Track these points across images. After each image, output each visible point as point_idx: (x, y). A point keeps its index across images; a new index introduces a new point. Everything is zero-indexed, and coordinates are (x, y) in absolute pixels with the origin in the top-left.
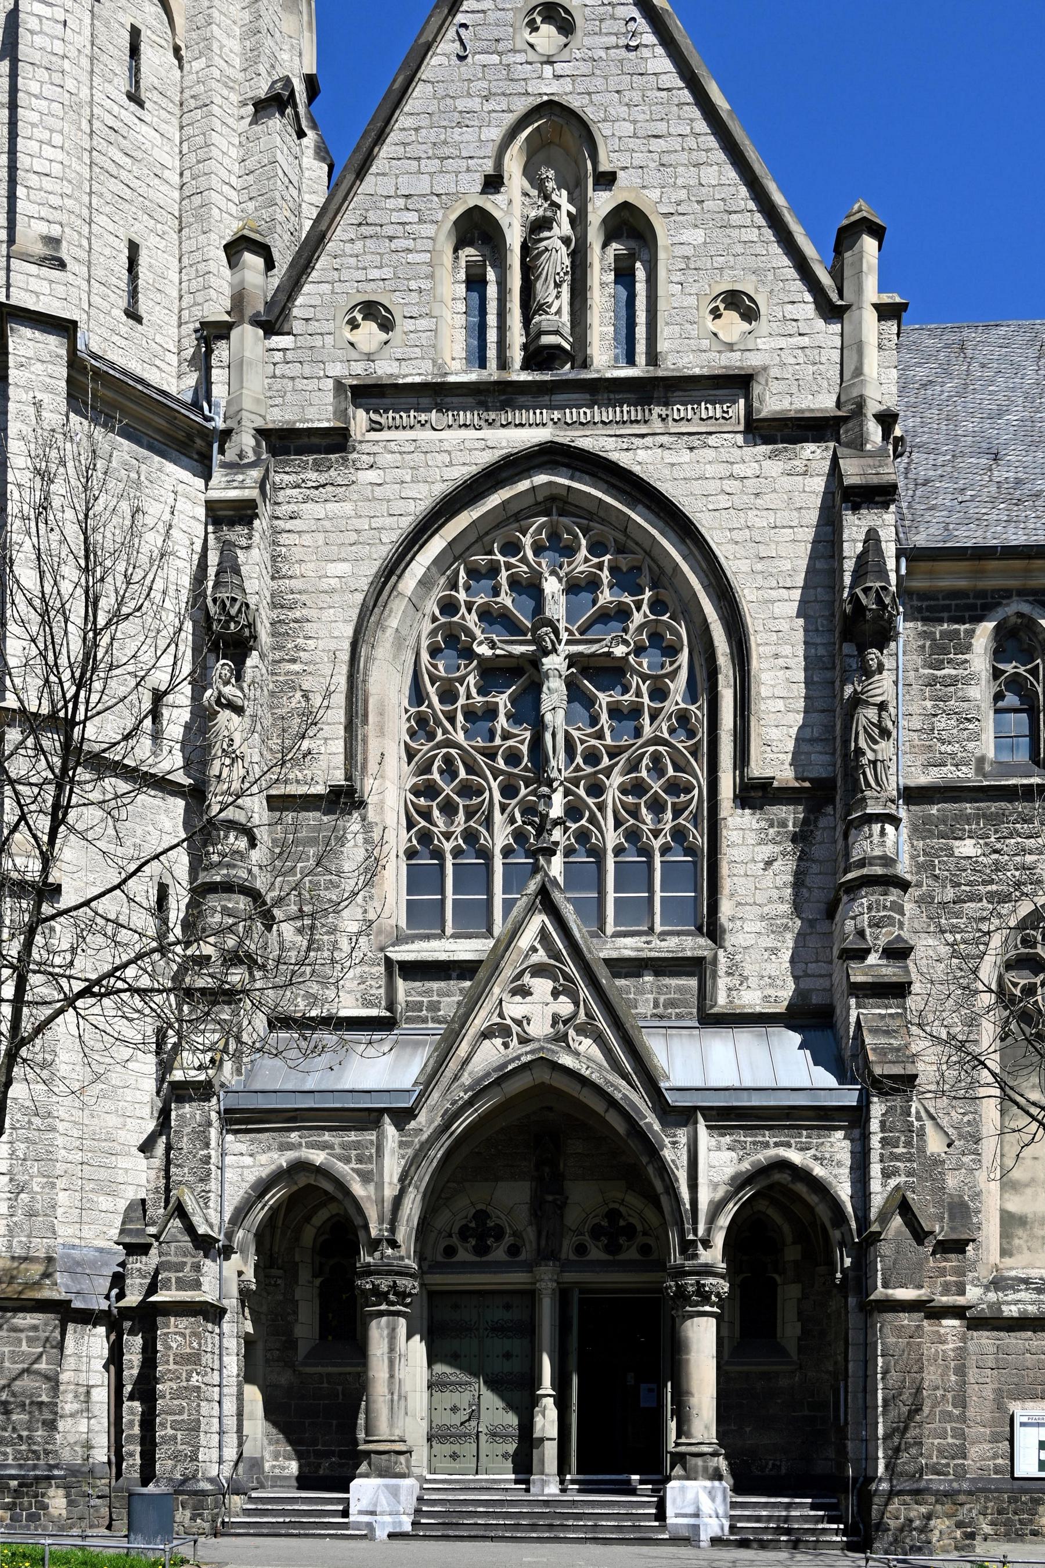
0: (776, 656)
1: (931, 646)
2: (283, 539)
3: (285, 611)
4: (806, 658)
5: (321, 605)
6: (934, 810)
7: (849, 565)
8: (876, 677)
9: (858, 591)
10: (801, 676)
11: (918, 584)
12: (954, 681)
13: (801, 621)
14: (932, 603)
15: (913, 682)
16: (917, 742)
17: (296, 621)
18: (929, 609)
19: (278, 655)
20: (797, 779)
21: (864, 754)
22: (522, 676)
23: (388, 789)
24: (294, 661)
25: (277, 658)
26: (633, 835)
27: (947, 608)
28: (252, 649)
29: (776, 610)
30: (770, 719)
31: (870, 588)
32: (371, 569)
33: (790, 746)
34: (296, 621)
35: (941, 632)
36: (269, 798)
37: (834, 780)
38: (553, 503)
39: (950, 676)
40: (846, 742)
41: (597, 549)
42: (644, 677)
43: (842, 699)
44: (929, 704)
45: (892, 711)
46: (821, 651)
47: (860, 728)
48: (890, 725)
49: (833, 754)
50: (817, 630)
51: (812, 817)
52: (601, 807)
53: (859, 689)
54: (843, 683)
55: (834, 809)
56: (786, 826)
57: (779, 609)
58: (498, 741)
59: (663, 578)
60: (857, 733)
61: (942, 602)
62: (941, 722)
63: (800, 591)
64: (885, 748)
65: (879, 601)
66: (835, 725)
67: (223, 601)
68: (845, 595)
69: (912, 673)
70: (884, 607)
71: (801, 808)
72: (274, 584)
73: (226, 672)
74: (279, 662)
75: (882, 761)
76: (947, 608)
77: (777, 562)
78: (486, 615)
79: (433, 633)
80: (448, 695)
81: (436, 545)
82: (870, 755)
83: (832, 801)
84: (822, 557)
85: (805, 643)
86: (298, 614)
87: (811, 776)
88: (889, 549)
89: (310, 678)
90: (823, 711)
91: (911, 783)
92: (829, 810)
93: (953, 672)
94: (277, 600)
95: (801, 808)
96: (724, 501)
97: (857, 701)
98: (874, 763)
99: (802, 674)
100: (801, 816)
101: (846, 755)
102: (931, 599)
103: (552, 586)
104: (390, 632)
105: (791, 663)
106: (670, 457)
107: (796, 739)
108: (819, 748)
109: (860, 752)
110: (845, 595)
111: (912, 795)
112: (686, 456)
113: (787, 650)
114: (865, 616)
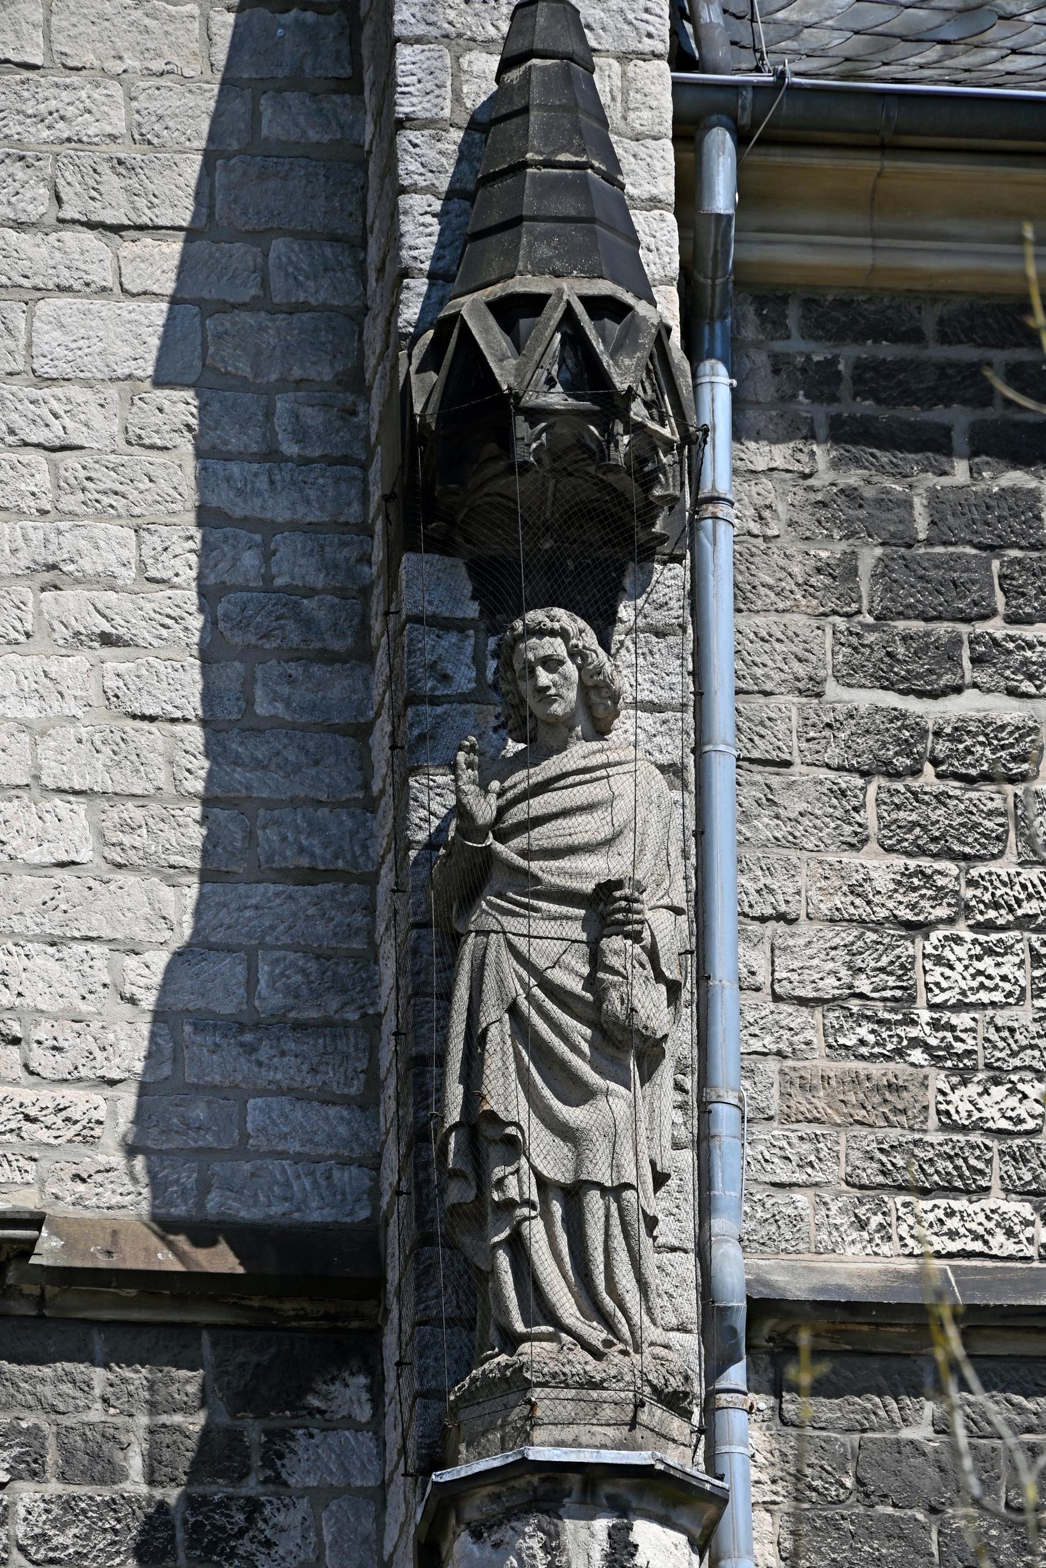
0: (51, 575)
1: (882, 571)
4: (209, 595)
7: (428, 161)
8: (578, 753)
9: (471, 307)
10: (185, 687)
11: (803, 253)
13: (181, 405)
14: (888, 351)
15: (794, 748)
16: (819, 1062)
18: (870, 378)
20: (165, 1226)
21: (514, 1147)
29: (48, 339)
31: (536, 303)
33: (129, 1047)
35: (935, 499)
37: (367, 1241)
39: (990, 730)
40: (422, 1069)
43: (400, 841)
44: (880, 867)
45: (669, 931)
46: (295, 564)
47: (492, 1012)
48: (651, 1006)
49: (367, 1103)
50: (271, 455)
51: (254, 1433)
53: (484, 809)
54: (411, 756)
55: (376, 1394)
56: (114, 1474)
57: (59, 331)
60: (476, 1040)
61: (937, 352)
62: (951, 968)
63: (174, 248)
64: (633, 1124)
65: (585, 373)
66: (372, 955)
68: (410, 312)
69: (789, 703)
70: (611, 405)
71: (188, 1382)
75: (616, 1191)
77: (49, 94)
82: (546, 1154)
83: (360, 1350)
84: (296, 82)
85: (205, 516)
87: (246, 1213)
88: (639, 97)
90: (309, 876)
91: (793, 1279)
92: (349, 1395)
93: (1009, 711)
95: (188, 1382)
97: (471, 872)
98: (573, 1194)
99: (190, 682)
100: (195, 1423)
101: (421, 1135)
102: (878, 332)
105: (127, 611)
107: (159, 1016)
108: (287, 1069)
109: (488, 1137)
110: (410, 312)
111: (789, 1340)
113: (108, 546)
114: (506, 440)
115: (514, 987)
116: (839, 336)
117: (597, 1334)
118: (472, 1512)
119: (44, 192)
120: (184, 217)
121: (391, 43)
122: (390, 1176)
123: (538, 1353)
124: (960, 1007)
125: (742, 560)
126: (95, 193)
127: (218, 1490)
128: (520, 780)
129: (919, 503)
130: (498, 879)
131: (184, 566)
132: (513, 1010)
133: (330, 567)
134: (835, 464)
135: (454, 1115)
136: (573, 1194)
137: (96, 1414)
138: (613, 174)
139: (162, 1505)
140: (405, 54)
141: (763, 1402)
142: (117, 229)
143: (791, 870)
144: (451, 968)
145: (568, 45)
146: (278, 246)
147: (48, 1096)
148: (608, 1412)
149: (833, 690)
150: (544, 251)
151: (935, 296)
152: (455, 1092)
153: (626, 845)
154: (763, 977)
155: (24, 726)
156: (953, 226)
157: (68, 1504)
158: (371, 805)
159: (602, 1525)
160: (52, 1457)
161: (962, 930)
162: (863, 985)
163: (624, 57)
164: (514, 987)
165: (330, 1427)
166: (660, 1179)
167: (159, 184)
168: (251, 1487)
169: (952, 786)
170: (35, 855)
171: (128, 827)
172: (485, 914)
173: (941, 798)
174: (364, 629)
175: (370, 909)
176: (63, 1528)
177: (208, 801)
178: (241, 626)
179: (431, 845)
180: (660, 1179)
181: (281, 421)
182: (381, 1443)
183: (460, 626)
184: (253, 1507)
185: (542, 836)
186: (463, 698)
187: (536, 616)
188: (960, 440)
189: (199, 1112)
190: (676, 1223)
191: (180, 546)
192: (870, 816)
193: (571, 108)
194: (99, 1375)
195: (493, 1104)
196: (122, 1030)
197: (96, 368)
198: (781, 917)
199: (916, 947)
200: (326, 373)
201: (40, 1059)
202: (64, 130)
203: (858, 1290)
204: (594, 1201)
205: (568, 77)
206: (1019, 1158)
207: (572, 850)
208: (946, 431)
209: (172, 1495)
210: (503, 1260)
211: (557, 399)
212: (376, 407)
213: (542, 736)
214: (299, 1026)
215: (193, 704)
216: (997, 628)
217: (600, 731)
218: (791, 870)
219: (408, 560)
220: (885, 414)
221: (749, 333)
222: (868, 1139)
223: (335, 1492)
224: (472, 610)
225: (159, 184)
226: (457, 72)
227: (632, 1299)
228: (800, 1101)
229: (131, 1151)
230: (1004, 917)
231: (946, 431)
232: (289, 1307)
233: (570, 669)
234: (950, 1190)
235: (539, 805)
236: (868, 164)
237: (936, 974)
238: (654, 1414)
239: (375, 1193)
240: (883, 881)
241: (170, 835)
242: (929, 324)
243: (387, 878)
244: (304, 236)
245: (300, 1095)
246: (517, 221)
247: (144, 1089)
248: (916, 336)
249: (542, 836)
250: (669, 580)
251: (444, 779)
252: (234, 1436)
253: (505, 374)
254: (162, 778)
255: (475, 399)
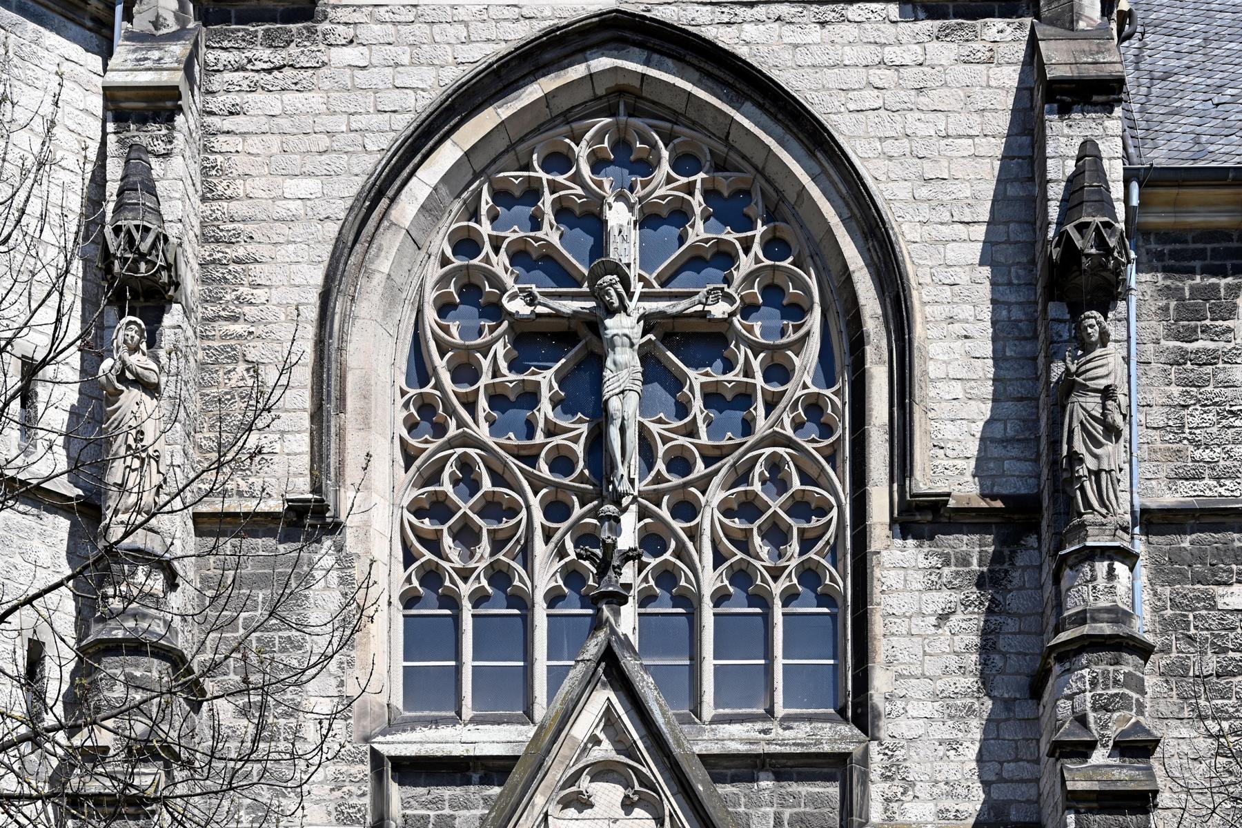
0: (951, 320)
1: (1177, 308)
2: (219, 143)
3: (222, 247)
4: (994, 323)
5: (276, 239)
6: (1186, 542)
7: (1056, 192)
8: (1098, 352)
9: (1069, 228)
10: (988, 349)
12: (1212, 358)
13: (986, 271)
14: (1178, 246)
15: (1152, 358)
16: (1158, 445)
17: (238, 261)
18: (1174, 254)
19: (211, 310)
20: (983, 496)
21: (1081, 461)
22: (574, 345)
23: (376, 506)
24: (234, 319)
25: (210, 314)
26: (741, 576)
27: (1200, 254)
28: (172, 300)
29: (950, 255)
30: (942, 410)
31: (1087, 224)
32: (350, 188)
33: (973, 448)
34: (238, 261)
35: (1191, 287)
36: (197, 517)
37: (1036, 499)
38: (621, 98)
39: (1206, 351)
40: (1055, 444)
41: (684, 163)
42: (756, 348)
43: (1048, 382)
44: (1175, 390)
45: (1123, 400)
46: (1017, 314)
47: (1076, 424)
48: (1119, 419)
49: (1037, 460)
50: (1010, 284)
52: (694, 534)
53: (1073, 368)
54: (1050, 360)
55: (1039, 540)
56: (968, 564)
57: (953, 252)
58: (539, 438)
59: (782, 206)
60: (1071, 432)
61: (1192, 246)
62: (1194, 417)
63: (984, 227)
64: (1112, 453)
65: (1101, 242)
67: (129, 232)
68: (1051, 234)
69: (1151, 346)
70: (1108, 251)
71: (989, 538)
72: (206, 208)
73: (133, 333)
74: (213, 320)
76: (1200, 254)
78: (520, 256)
79: (443, 281)
80: (465, 371)
81: (447, 155)
82: (1091, 463)
83: (1036, 529)
84: (1016, 179)
85: (993, 301)
86: (241, 252)
87: (1004, 492)
88: (1115, 170)
89: (259, 344)
90: (1021, 399)
91: (1152, 503)
92: (1032, 540)
94: (209, 231)
95: (989, 538)
96: (871, 99)
97: (1070, 386)
98: (1097, 474)
100: (991, 549)
101: (1055, 463)
102: (1176, 241)
103: (618, 216)
104: (378, 279)
105: (972, 329)
106: (790, 34)
107: (982, 439)
108: (1015, 451)
109: (1075, 458)
110: (1051, 234)
111: (1154, 521)
112: (815, 34)
113: (966, 311)
114: (1080, 263)
115: (1082, 416)
116: (1165, 243)
117: (1104, 511)
118: (1070, 562)
119: (948, 214)
120: (987, 219)
121: (1045, 159)
122: (1044, 477)
123: (1088, 517)
124: (1197, 428)
125: (1139, 307)
126: (962, 214)
127: (997, 567)
128: (1083, 360)
129: (1187, 289)
130: (1077, 387)
131: (987, 315)
132: (1081, 423)
133: (1026, 314)
134: (1164, 279)
135: (1065, 453)
136: (1097, 474)
137: (964, 548)
138: (1108, 189)
139: (982, 572)
140: (1049, 162)
141: (1144, 538)
142: (968, 223)
143: (1151, 392)
144: (1063, 417)
145: (1096, 153)
146: (1012, 225)
147: (951, 462)
148: (1107, 532)
149: (1163, 342)
150: (1090, 210)
151: (1191, 230)
152: (1065, 447)
153: (1112, 376)
154: (1143, 422)
155: (944, 362)
156: (1197, 209)
157: (957, 573)
158: (1037, 379)
159: (1106, 563)
160: (953, 560)
161: (1198, 406)
162: (1171, 423)
163: (1110, 159)
164: (1082, 416)
165: (1026, 549)
166: (1121, 470)
167: (979, 210)
168: (1006, 566)
169: (1195, 367)
170: (947, 397)
171: (972, 388)
172: (1073, 398)
173: (1192, 370)
174: (1036, 329)
175: (1037, 407)
176: (955, 579)
177: (994, 380)
178: (1002, 331)
179: (1057, 382)
180: (1121, 470)
181: (1013, 274)
182: (1040, 552)
183: (1064, 321)
184: (1006, 572)
185: (1089, 374)
186: (1065, 341)
187: (1088, 313)
188: (1198, 270)
189: (992, 465)
190: (1124, 484)
191: (986, 310)
192: (1172, 376)
193: (1097, 170)
194: (965, 537)
195: (1076, 449)
196: (971, 443)
197: (962, 262)
198: (1148, 405)
199: (1185, 412)
200: (1024, 260)
201: (949, 452)
202: (953, 196)
203: (1169, 505)
204: (1104, 475)
205: (1096, 162)
206: (1213, 469)
207: (1097, 378)
208: (1194, 268)
209: (985, 569)
210: (1078, 493)
211: (1093, 251)
212: (1039, 267)
213: (1087, 347)
214: (1019, 440)
215: (990, 354)
216: (1208, 322)
217: (1104, 346)
218: (1151, 392)
219: (1050, 304)
220: (1177, 264)
221: (1140, 243)
222: (1172, 465)
223: (1028, 567)
224: (1068, 317)
225: (979, 210)
226: (1064, 166)
227: (1114, 502)
228: (1153, 456)
229: (974, 476)
230: (1209, 403)
231: (1194, 268)
232: (1016, 517)
233: (1097, 327)
234: (1194, 479)
235: (1089, 366)
236: (1174, 191)
237: (1191, 419)
238: (1120, 533)
239: (1039, 485)
240: (1176, 394)
241: (983, 390)
242: (1190, 239)
243: (1043, 396)
244: (1019, 222)
245: (1019, 459)
246: (1081, 203)
247: (977, 459)
248: (1186, 242)
249: (1089, 374)
250: (1121, 305)
251: (1061, 364)
252: (1001, 552)
253: (1079, 244)
254: (981, 374)
255: (1071, 252)
